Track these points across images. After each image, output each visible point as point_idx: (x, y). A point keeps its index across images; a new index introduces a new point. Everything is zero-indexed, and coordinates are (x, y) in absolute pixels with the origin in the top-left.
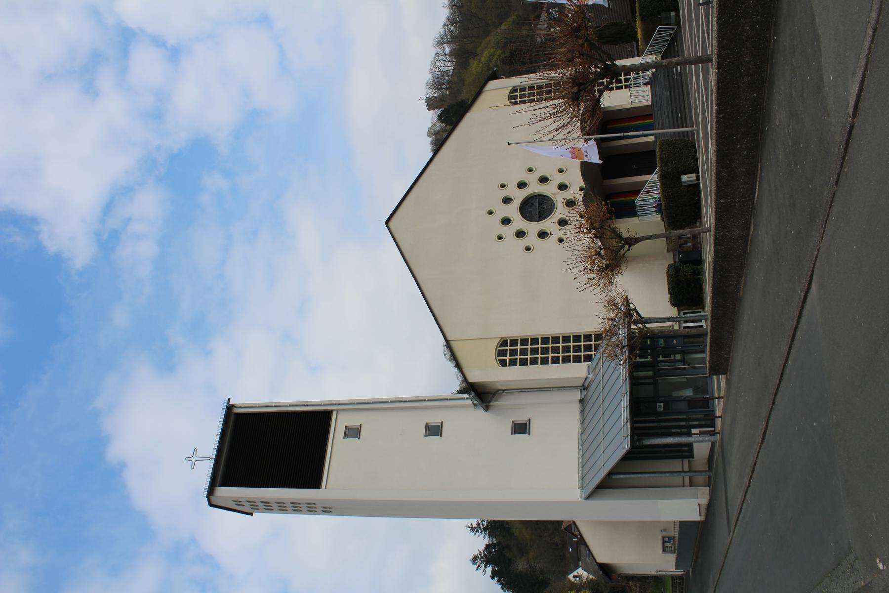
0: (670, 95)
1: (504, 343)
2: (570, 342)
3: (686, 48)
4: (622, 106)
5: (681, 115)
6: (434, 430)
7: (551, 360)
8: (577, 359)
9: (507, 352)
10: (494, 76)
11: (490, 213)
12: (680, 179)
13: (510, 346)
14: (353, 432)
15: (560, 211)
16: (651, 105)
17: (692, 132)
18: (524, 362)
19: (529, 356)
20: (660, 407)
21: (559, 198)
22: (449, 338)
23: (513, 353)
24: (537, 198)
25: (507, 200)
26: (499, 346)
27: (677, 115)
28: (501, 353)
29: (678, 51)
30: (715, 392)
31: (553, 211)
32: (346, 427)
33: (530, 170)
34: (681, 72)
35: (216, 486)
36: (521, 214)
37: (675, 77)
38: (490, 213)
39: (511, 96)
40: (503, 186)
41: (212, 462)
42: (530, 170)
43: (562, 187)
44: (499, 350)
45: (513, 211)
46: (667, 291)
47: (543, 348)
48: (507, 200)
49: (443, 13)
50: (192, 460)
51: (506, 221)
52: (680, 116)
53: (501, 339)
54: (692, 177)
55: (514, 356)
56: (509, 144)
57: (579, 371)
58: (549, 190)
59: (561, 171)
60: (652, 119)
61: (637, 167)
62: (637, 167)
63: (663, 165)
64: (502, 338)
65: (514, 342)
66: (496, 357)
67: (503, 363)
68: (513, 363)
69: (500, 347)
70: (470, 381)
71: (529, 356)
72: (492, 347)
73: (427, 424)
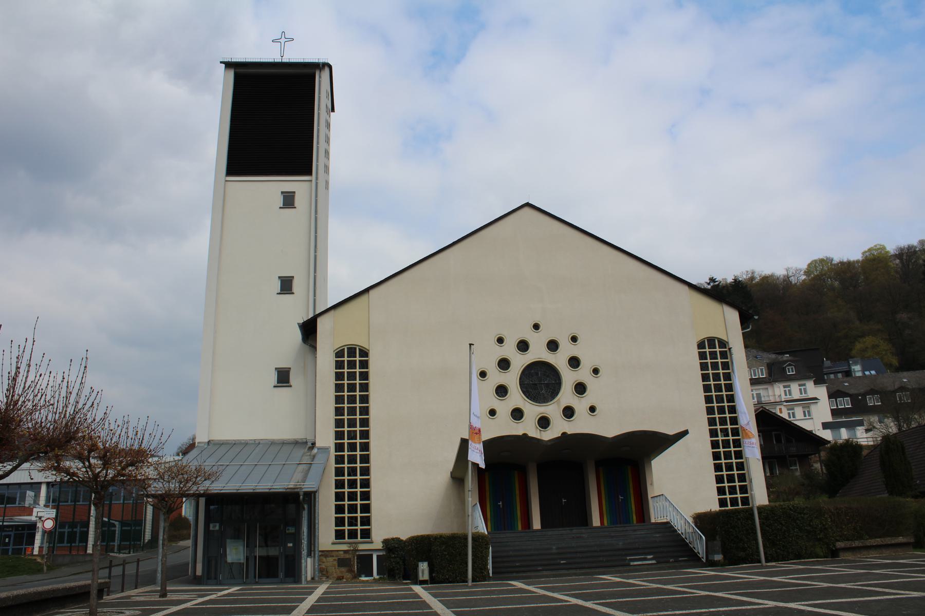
0: (619, 550)
1: (364, 353)
2: (718, 414)
3: (782, 564)
4: (652, 484)
5: (564, 564)
6: (286, 285)
7: (340, 407)
8: (339, 435)
9: (353, 357)
10: (745, 320)
11: (536, 327)
12: (423, 560)
13: (719, 351)
14: (289, 200)
15: (532, 411)
16: (651, 523)
17: (759, 561)
18: (339, 376)
19: (710, 372)
20: (215, 527)
21: (552, 410)
22: (372, 292)
23: (352, 365)
24: (555, 381)
25: (553, 346)
26: (360, 348)
27: (563, 559)
28: (352, 351)
29: (668, 562)
30: (222, 586)
31: (534, 402)
32: (294, 192)
33: (596, 371)
34: (629, 565)
35: (235, 69)
36: (532, 363)
37: (628, 558)
38: (536, 327)
39: (714, 340)
40: (574, 339)
41: (278, 60)
42: (596, 371)
43: (569, 412)
44: (355, 348)
45: (538, 353)
46: (413, 535)
47: (356, 398)
48: (553, 346)
49: (912, 240)
50: (284, 39)
51: (523, 346)
52: (562, 562)
53: (367, 350)
54: (423, 576)
55: (347, 366)
56: (471, 345)
57: (326, 438)
58: (567, 396)
59: (592, 409)
60: (637, 522)
61: (563, 504)
62: (563, 504)
63: (444, 540)
64: (728, 343)
65: (364, 364)
66: (360, 346)
67: (339, 354)
68: (339, 365)
69: (359, 349)
70: (319, 320)
71: (710, 372)
72: (359, 341)
73: (293, 277)
